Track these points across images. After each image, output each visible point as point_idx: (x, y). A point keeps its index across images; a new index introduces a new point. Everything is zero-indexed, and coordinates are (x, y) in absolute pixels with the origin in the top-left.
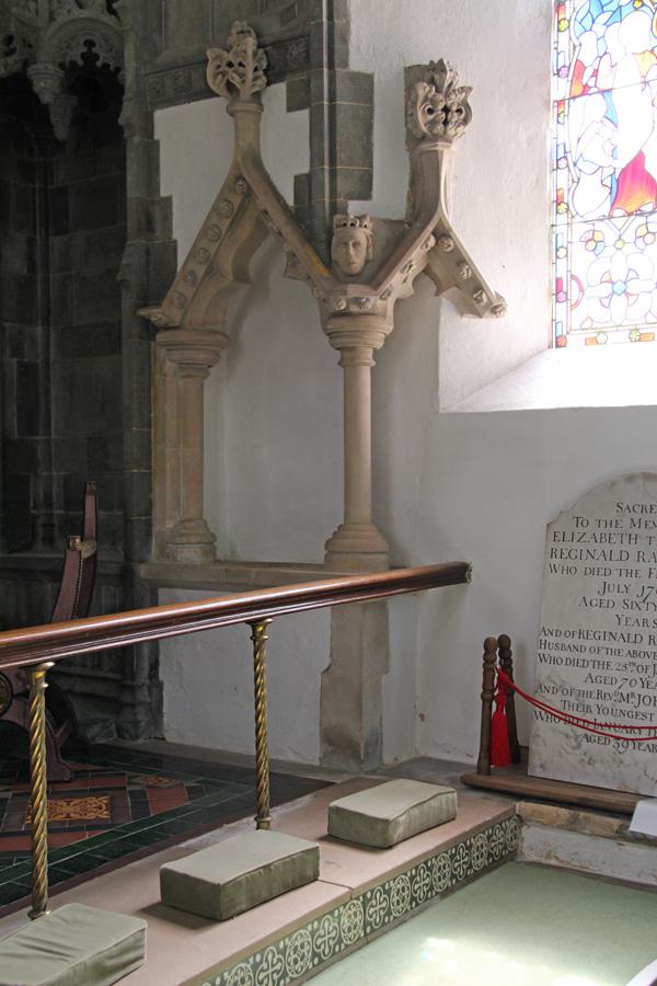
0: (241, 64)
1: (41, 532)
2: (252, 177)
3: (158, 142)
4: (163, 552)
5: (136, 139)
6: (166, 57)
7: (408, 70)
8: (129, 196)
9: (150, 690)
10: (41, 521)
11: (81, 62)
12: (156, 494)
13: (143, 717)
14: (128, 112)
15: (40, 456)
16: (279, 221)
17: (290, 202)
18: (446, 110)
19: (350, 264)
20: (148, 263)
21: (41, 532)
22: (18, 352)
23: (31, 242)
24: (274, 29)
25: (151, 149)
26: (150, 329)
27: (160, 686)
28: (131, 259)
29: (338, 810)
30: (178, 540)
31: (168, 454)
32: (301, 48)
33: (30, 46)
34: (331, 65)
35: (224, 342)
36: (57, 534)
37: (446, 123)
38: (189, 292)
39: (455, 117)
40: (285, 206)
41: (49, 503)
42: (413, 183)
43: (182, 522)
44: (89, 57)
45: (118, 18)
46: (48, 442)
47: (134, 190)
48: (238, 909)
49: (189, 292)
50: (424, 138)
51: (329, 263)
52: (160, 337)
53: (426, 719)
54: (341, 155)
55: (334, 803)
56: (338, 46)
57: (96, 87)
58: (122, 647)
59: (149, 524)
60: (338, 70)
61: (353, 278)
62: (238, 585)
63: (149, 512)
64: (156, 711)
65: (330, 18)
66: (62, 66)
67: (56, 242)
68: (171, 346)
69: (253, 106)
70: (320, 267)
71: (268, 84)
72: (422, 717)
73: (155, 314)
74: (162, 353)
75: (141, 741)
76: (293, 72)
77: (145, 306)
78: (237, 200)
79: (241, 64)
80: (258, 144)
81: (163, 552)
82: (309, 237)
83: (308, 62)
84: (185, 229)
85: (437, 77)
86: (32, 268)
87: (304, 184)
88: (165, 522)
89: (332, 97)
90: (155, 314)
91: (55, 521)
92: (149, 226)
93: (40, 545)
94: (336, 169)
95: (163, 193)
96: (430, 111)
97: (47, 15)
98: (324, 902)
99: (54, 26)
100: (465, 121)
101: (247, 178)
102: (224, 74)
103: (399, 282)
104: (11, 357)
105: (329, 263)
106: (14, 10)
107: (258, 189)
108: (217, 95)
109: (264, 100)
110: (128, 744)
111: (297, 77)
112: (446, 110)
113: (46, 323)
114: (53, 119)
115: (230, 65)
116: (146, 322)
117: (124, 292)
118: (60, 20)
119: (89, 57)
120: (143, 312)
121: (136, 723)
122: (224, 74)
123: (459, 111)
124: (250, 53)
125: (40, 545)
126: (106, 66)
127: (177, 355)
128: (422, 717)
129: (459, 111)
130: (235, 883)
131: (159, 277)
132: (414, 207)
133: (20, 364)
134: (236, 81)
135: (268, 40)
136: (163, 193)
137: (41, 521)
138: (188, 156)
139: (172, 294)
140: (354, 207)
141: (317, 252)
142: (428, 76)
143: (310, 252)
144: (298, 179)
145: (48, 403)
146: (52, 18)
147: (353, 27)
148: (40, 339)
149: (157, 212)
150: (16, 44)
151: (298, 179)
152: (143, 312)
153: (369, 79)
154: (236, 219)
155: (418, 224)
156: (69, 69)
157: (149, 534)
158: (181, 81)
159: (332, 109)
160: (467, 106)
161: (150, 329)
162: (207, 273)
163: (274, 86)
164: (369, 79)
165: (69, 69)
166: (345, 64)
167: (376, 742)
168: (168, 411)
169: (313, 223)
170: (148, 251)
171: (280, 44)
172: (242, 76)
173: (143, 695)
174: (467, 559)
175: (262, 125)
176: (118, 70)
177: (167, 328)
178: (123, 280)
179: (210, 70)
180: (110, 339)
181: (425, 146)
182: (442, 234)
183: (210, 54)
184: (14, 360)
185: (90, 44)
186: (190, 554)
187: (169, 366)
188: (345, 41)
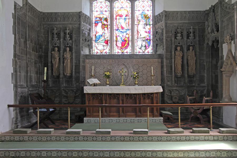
12: (223, 92)
22: (215, 73)
38: (225, 67)
48: (154, 43)
49: (225, 67)
52: (223, 73)
59: (222, 96)
68: (224, 74)
73: (222, 70)
74: (223, 74)
75: (220, 123)
80: (231, 48)
84: (224, 60)
90: (222, 70)
94: (26, 74)
104: (214, 74)
114: (215, 46)
118: (212, 36)
127: (225, 75)
133: (215, 75)
139: (223, 67)
146: (211, 36)
152: (221, 69)
172: (227, 41)
179: (225, 40)
183: (225, 38)
184: (214, 75)
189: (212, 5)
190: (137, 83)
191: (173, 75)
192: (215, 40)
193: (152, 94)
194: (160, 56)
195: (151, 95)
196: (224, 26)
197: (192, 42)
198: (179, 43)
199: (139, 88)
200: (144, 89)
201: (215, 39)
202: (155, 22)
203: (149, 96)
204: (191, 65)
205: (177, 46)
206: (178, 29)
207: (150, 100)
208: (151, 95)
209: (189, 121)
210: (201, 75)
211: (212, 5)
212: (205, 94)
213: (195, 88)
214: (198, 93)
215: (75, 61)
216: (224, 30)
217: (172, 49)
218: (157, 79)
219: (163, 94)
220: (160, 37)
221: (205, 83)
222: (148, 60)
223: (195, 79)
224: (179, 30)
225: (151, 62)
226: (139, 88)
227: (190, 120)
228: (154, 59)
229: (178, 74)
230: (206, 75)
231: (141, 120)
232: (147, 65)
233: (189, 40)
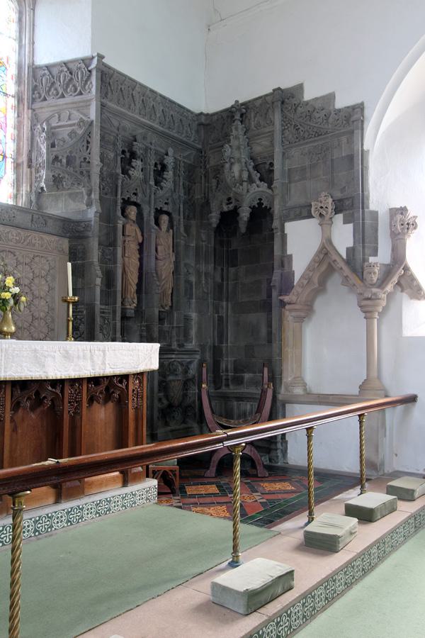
0: (326, 207)
1: (224, 381)
2: (329, 248)
3: (286, 234)
4: (287, 389)
5: (279, 233)
6: (290, 204)
7: (391, 210)
8: (275, 254)
9: (282, 444)
10: (224, 378)
11: (257, 206)
13: (280, 454)
14: (276, 224)
15: (224, 352)
16: (342, 264)
17: (345, 257)
18: (408, 224)
19: (372, 280)
20: (281, 279)
21: (224, 381)
23: (222, 270)
24: (338, 195)
25: (284, 237)
26: (283, 304)
27: (286, 442)
28: (276, 277)
29: (391, 486)
30: (294, 385)
31: (289, 352)
32: (350, 201)
33: (238, 201)
34: (363, 208)
35: (309, 309)
36: (230, 383)
37: (408, 229)
39: (411, 227)
40: (343, 258)
41: (227, 371)
42: (393, 250)
43: (295, 378)
44: (260, 204)
45: (272, 190)
46: (227, 347)
47: (277, 252)
50: (399, 234)
51: (362, 279)
53: (398, 455)
54: (367, 240)
55: (389, 484)
56: (365, 201)
57: (261, 214)
58: (122, 448)
59: (281, 379)
60: (366, 210)
61: (373, 285)
62: (339, 403)
63: (281, 375)
64: (285, 452)
65: (363, 191)
66: (250, 207)
67: (232, 270)
68: (290, 310)
69: (330, 222)
70: (360, 282)
71: (335, 214)
72: (396, 455)
73: (286, 299)
74: (287, 313)
76: (346, 210)
77: (281, 295)
78: (322, 256)
79: (326, 207)
81: (287, 389)
82: (354, 270)
83: (352, 206)
85: (404, 213)
86: (222, 280)
87: (351, 251)
88: (288, 377)
89: (363, 220)
90: (286, 299)
91: (230, 378)
92: (282, 265)
93: (224, 388)
95: (289, 253)
96: (402, 225)
97: (246, 191)
98: (404, 518)
99: (249, 194)
100: (415, 228)
101: (325, 251)
102: (319, 210)
103: (389, 288)
105: (362, 279)
106: (233, 189)
107: (332, 252)
108: (314, 217)
109: (333, 220)
110: (276, 465)
111: (347, 212)
112: (408, 224)
113: (227, 301)
115: (322, 207)
116: (281, 301)
117: (273, 290)
118: (251, 192)
119: (260, 204)
120: (281, 298)
121: (277, 457)
122: (319, 210)
123: (413, 224)
124: (330, 203)
125: (224, 388)
126: (266, 207)
127: (293, 314)
128: (396, 455)
129: (413, 224)
130: (377, 508)
131: (287, 285)
132: (394, 259)
133: (218, 316)
134: (324, 213)
135: (336, 199)
136: (289, 253)
137: (224, 378)
138: (301, 241)
140: (372, 259)
141: (358, 276)
142: (400, 212)
143: (355, 276)
144: (348, 249)
145: (227, 328)
146: (248, 191)
147: (371, 194)
148: (225, 307)
149: (286, 260)
150: (233, 200)
151: (348, 249)
152: (281, 298)
153: (377, 212)
154: (321, 262)
155: (397, 266)
156: (253, 208)
157: (281, 383)
158: (298, 213)
159: (363, 224)
160: (416, 224)
161: (283, 304)
162: (308, 282)
163: (337, 215)
164: (377, 212)
165: (253, 208)
166: (368, 208)
167: (383, 464)
168: (288, 335)
169: (356, 263)
170: (282, 275)
171: (340, 200)
173: (279, 446)
174: (415, 393)
175: (332, 229)
176: (270, 208)
177: (290, 304)
178: (274, 286)
180: (266, 306)
181: (400, 237)
182: (406, 269)
183: (313, 204)
185: (260, 199)
186: (298, 391)
187: (290, 318)
188: (368, 199)
189: (237, 102)
190: (13, 328)
191: (117, 305)
192: (257, 206)
193: (124, 377)
194: (73, 231)
195: (121, 382)
196: (289, 170)
197: (168, 200)
198: (135, 194)
199: (81, 354)
200: (101, 358)
201: (258, 204)
202: (35, 88)
203: (108, 388)
204: (163, 277)
205: (127, 202)
206: (136, 141)
207: (110, 405)
208: (120, 385)
209: (208, 473)
210: (133, 316)
211: (237, 102)
212: (194, 376)
213: (173, 356)
214: (176, 375)
215: (131, 138)
216: (290, 182)
217: (116, 211)
218: (53, 321)
219: (160, 379)
220: (71, 152)
221: (191, 342)
222: (22, 233)
223: (166, 325)
224: (138, 148)
225: (34, 245)
226: (81, 354)
227: (212, 471)
228: (44, 236)
229: (128, 307)
230: (194, 315)
231: (82, 509)
232: (17, 253)
233: (160, 193)
